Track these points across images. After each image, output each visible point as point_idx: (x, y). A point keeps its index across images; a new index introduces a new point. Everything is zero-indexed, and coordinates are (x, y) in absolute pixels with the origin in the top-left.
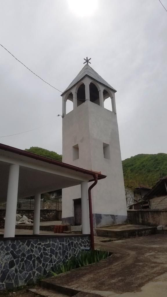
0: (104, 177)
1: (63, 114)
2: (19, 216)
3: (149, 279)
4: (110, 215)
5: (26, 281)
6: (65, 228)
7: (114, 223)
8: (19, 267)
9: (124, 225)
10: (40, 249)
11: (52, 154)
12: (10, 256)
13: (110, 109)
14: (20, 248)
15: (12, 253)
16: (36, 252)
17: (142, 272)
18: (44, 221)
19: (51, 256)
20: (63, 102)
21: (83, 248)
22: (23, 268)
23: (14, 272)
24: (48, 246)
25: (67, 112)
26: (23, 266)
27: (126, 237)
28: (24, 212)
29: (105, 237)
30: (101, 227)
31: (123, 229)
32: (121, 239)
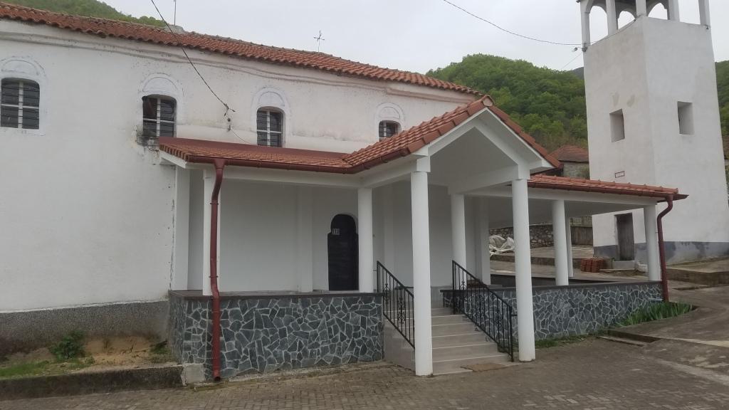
0: (684, 197)
1: (585, 44)
2: (500, 239)
3: (184, 31)
4: (693, 243)
5: (587, 330)
6: (601, 266)
7: (700, 256)
8: (579, 316)
9: (723, 259)
10: (597, 298)
11: (519, 67)
12: (569, 304)
14: (578, 297)
15: (570, 301)
16: (594, 302)
18: (546, 246)
19: (611, 307)
20: (584, 17)
21: (652, 299)
22: (582, 317)
23: (574, 321)
24: (607, 295)
25: (594, 38)
26: (583, 316)
27: (724, 283)
28: (507, 230)
29: (682, 282)
30: (674, 265)
31: (719, 268)
32: (714, 287)
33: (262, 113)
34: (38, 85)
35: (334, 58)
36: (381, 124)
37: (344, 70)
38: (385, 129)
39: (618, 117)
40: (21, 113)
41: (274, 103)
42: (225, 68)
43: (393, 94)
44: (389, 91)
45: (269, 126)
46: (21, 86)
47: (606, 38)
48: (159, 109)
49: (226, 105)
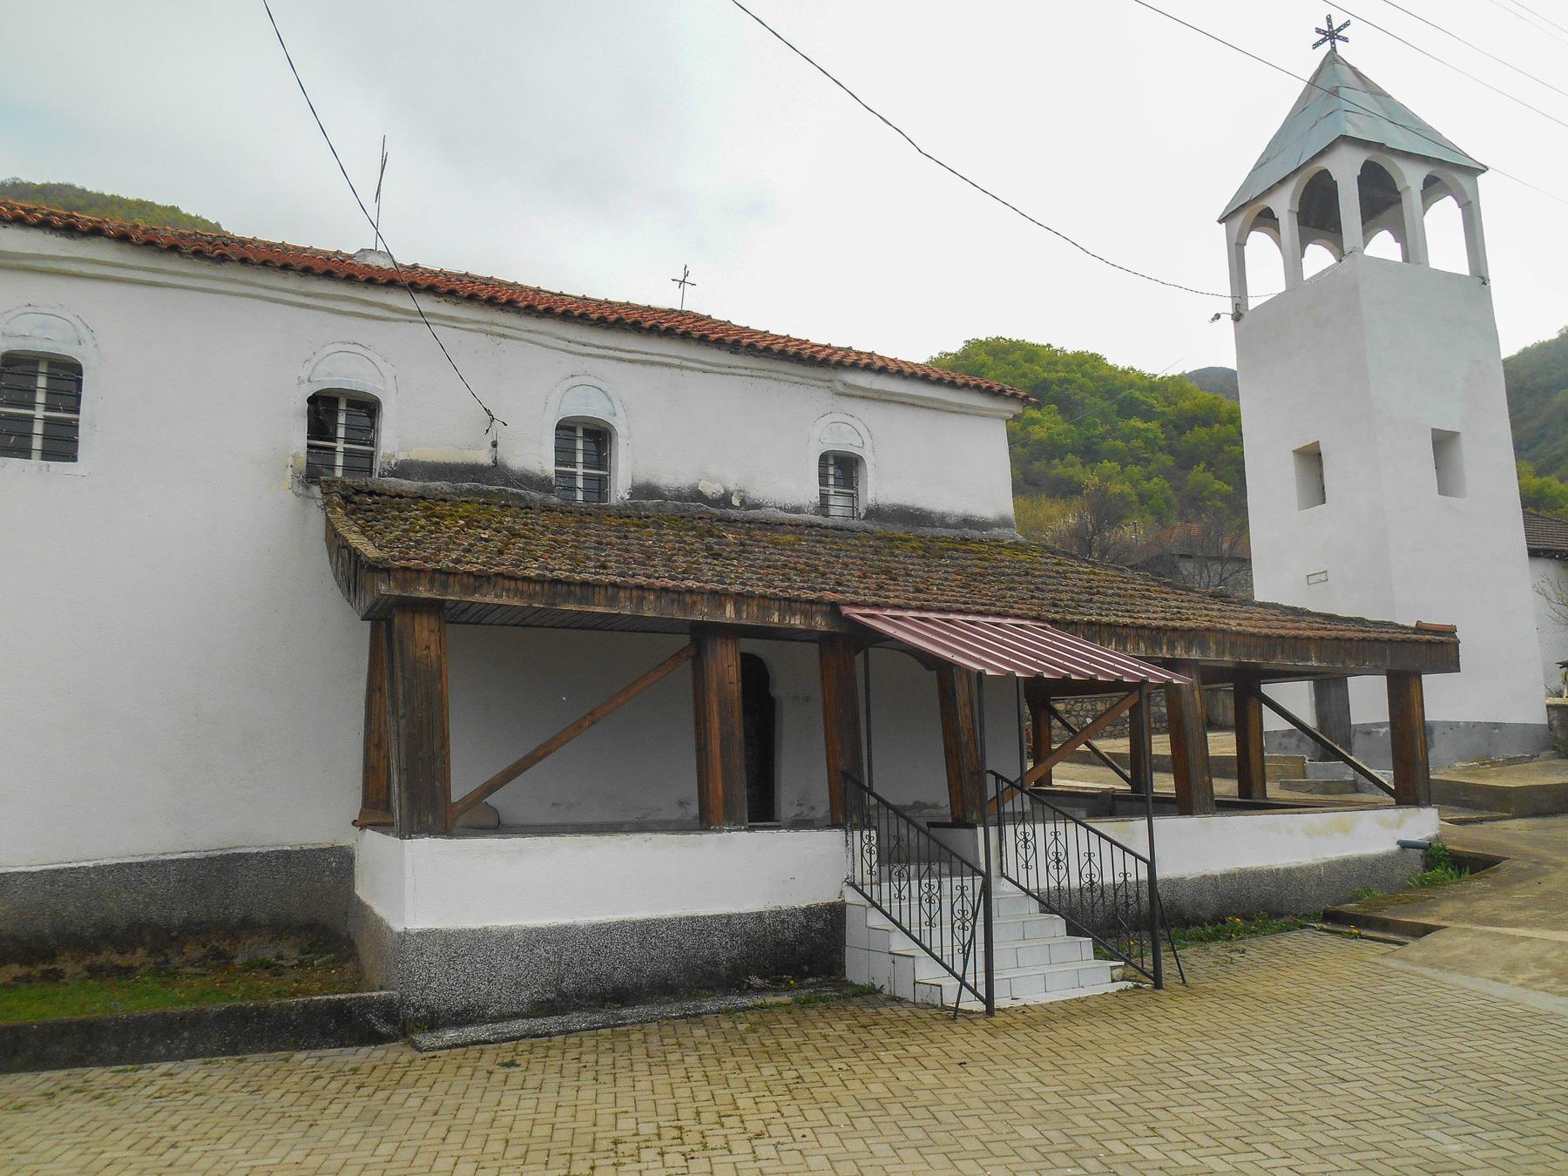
1: (1237, 306)
13: (1459, 264)
17: (1181, 387)
33: (566, 429)
34: (79, 367)
35: (715, 322)
36: (824, 458)
37: (745, 341)
38: (831, 471)
39: (1311, 458)
40: (38, 428)
41: (594, 408)
42: (487, 333)
43: (848, 396)
44: (840, 388)
45: (580, 458)
46: (43, 368)
47: (1453, 196)
48: (342, 419)
49: (488, 412)
